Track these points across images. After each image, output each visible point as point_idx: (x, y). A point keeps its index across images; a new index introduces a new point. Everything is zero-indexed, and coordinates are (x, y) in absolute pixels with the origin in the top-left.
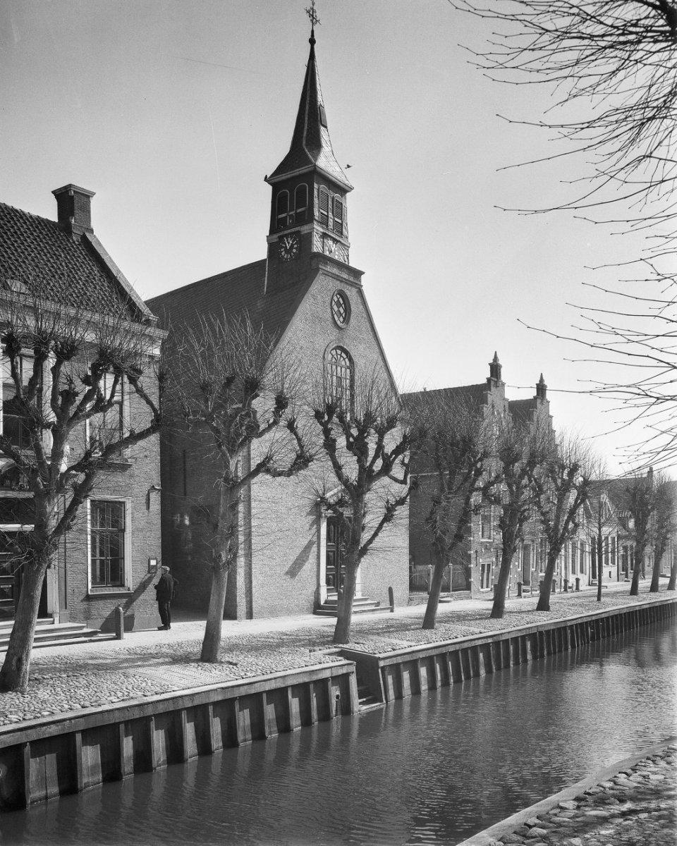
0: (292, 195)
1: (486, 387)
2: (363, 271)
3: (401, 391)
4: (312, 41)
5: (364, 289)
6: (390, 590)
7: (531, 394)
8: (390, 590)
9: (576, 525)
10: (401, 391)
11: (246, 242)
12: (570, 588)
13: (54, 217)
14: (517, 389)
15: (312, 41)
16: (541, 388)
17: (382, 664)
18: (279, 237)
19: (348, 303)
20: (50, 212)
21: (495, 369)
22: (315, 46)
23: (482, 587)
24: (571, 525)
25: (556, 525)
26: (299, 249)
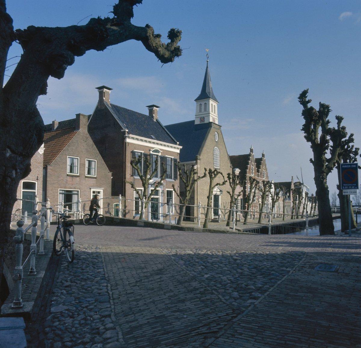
6: (292, 177)
7: (260, 156)
8: (292, 177)
14: (257, 155)
20: (146, 112)
21: (251, 150)
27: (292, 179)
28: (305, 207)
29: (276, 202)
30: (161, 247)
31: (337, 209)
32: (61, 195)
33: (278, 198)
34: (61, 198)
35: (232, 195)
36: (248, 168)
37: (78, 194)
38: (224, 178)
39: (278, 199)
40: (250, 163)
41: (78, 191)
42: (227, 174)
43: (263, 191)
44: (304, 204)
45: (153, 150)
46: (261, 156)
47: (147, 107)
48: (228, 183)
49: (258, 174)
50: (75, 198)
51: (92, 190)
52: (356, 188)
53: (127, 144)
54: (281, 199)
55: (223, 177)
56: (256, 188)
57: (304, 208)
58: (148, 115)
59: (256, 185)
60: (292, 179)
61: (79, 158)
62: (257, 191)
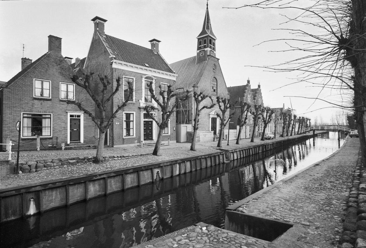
0: (203, 41)
1: (247, 85)
2: (216, 50)
3: (227, 87)
4: (207, 5)
5: (219, 63)
6: (284, 104)
7: (257, 87)
8: (284, 104)
9: (271, 120)
10: (227, 87)
11: (193, 52)
12: (256, 136)
13: (150, 48)
14: (254, 86)
15: (207, 5)
16: (259, 86)
17: (230, 151)
18: (200, 51)
19: (216, 67)
20: (149, 46)
21: (249, 82)
22: (208, 6)
23: (146, 78)
24: (269, 120)
25: (266, 119)
26: (205, 54)
27: (284, 106)
28: (294, 127)
29: (268, 123)
30: (274, 140)
31: (327, 127)
32: (25, 120)
33: (269, 120)
34: (27, 122)
35: (222, 118)
36: (245, 96)
37: (50, 118)
38: (213, 102)
39: (270, 121)
40: (247, 92)
41: (51, 115)
42: (217, 98)
43: (255, 114)
44: (293, 125)
45: (145, 77)
46: (247, 83)
47: (150, 41)
48: (217, 106)
49: (254, 101)
50: (46, 123)
51: (69, 114)
52: (57, 43)
53: (114, 70)
54: (273, 121)
55: (212, 100)
56: (248, 111)
57: (293, 128)
58: (151, 49)
59: (248, 108)
60: (284, 106)
61: (51, 81)
62: (249, 114)
